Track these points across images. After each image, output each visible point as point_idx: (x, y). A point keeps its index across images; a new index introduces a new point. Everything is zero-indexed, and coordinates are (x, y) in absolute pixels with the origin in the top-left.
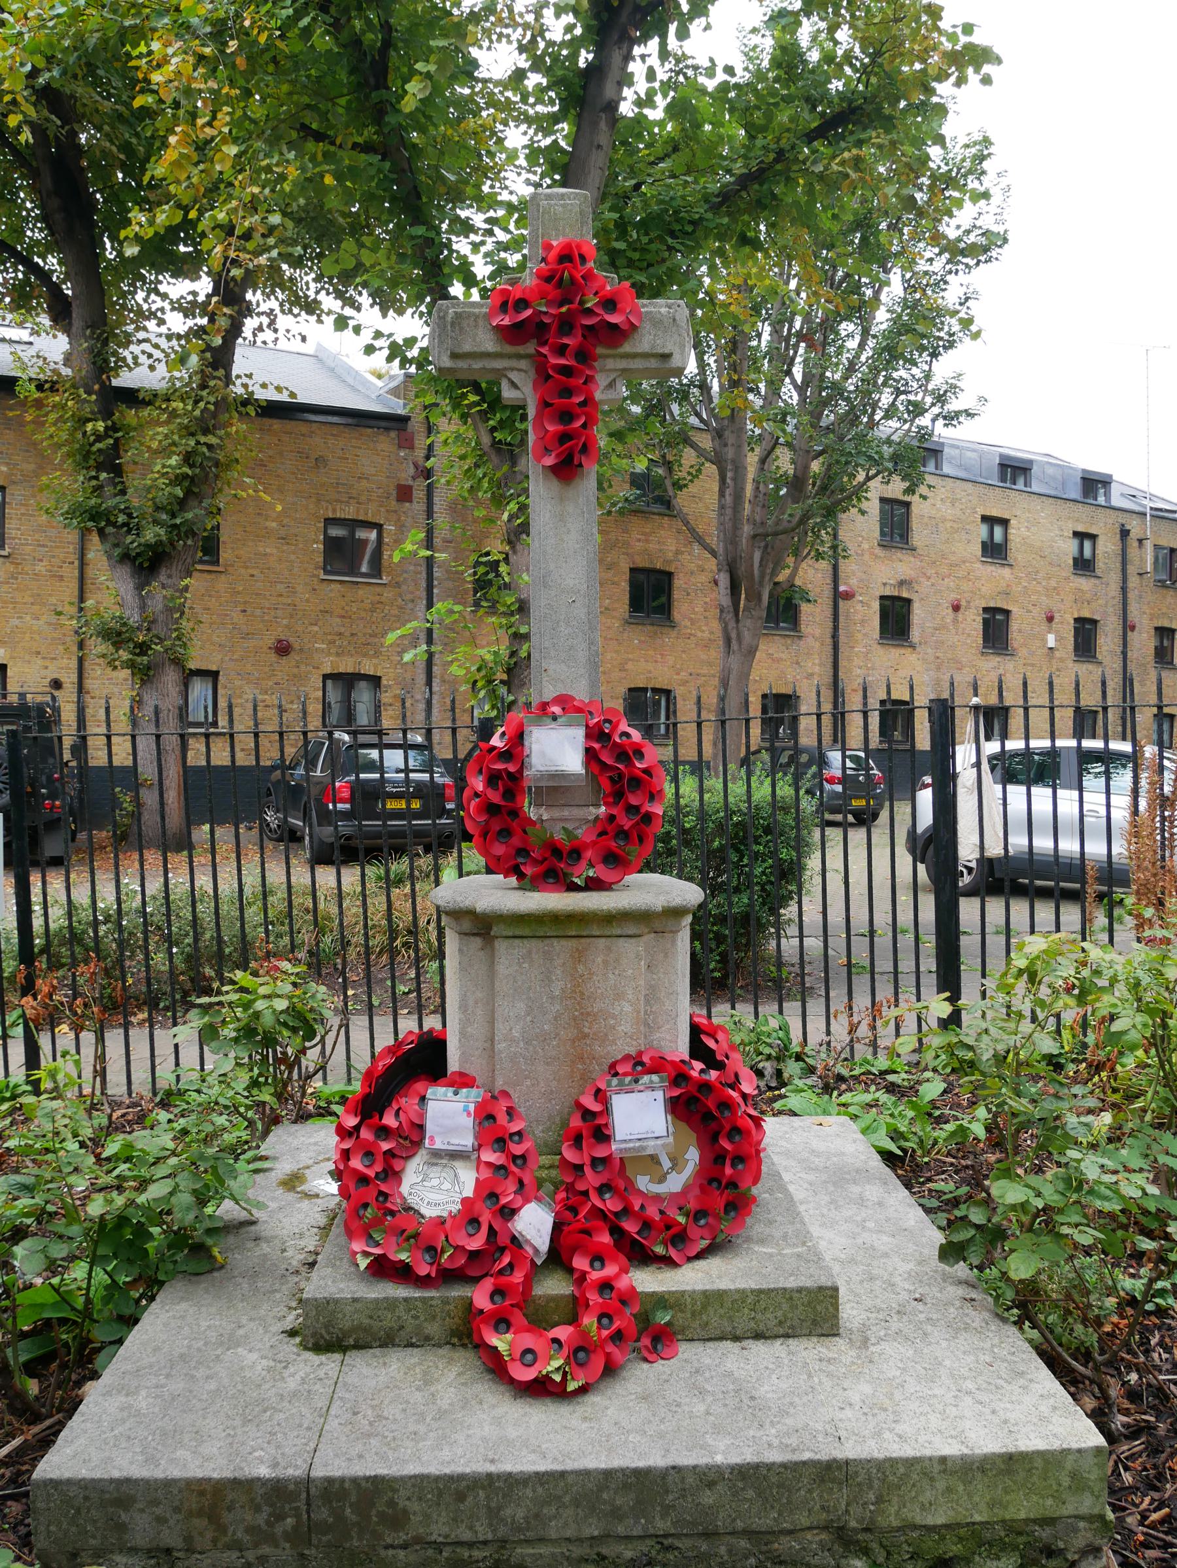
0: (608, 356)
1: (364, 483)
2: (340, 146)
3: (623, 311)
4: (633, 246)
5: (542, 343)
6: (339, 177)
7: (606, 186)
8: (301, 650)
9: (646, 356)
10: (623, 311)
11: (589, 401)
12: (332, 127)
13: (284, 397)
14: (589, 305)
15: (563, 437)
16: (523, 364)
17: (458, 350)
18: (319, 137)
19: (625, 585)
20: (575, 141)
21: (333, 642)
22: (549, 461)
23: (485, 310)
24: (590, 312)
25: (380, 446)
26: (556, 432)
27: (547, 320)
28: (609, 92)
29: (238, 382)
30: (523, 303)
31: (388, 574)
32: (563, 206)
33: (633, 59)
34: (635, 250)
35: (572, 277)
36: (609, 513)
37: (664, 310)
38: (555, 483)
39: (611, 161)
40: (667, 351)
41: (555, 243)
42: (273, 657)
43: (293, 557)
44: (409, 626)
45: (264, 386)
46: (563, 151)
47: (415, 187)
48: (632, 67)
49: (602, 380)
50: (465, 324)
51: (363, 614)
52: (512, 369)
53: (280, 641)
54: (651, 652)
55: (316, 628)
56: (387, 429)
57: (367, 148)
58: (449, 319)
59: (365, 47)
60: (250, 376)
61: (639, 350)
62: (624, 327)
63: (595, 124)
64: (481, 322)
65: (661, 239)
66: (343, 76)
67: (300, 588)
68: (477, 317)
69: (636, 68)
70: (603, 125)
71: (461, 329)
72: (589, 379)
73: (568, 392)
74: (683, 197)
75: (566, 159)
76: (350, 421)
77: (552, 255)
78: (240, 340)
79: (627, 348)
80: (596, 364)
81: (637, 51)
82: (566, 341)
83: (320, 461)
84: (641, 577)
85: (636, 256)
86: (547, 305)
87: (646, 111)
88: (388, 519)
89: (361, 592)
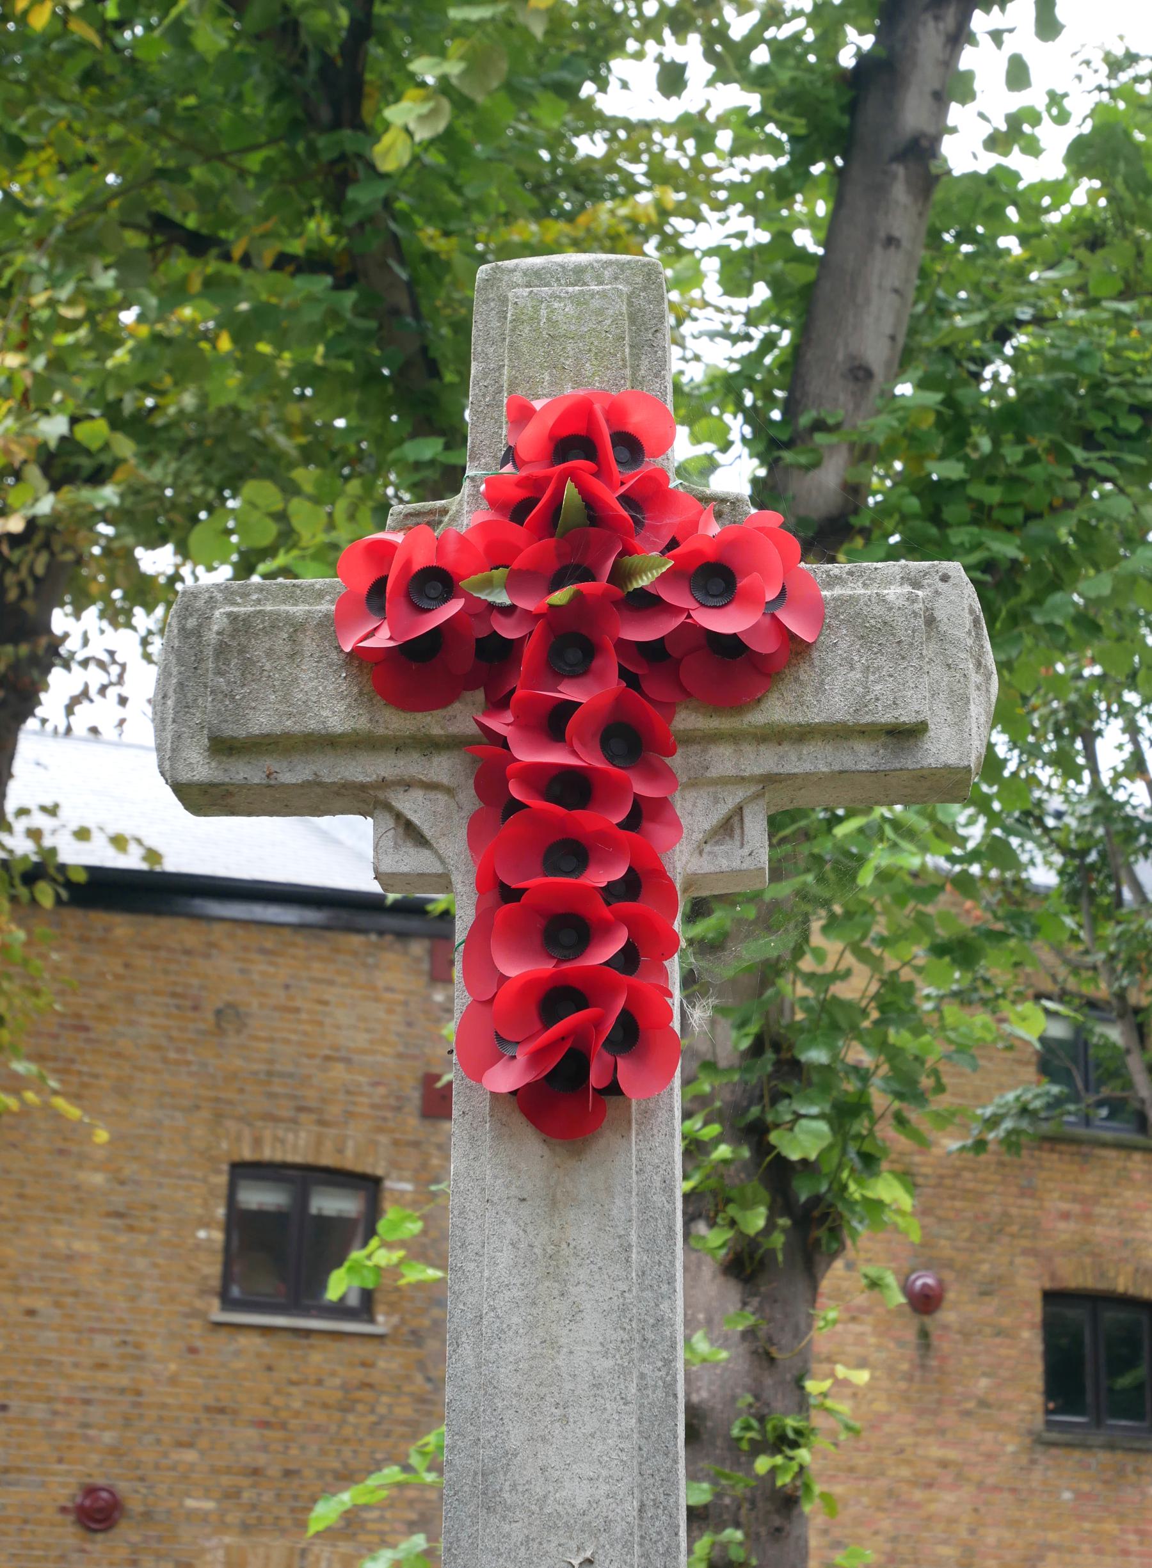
0: (714, 738)
1: (339, 1071)
2: (246, 261)
3: (752, 598)
4: (983, 470)
5: (497, 704)
6: (242, 331)
7: (912, 332)
8: (147, 1516)
9: (838, 733)
10: (752, 598)
11: (644, 880)
12: (228, 224)
13: (132, 860)
14: (644, 581)
15: (556, 998)
16: (442, 768)
17: (230, 730)
18: (198, 244)
19: (1031, 1339)
20: (831, 234)
21: (232, 1494)
22: (507, 1077)
23: (327, 607)
24: (647, 603)
25: (383, 979)
26: (529, 985)
27: (509, 631)
28: (913, 115)
29: (20, 825)
30: (437, 581)
31: (393, 1308)
32: (576, 300)
33: (971, 39)
34: (991, 481)
35: (590, 500)
36: (980, 1145)
37: (895, 593)
38: (532, 1149)
39: (923, 274)
40: (906, 717)
41: (538, 405)
42: (69, 1534)
43: (141, 1263)
44: (373, 1481)
45: (82, 834)
46: (801, 255)
47: (424, 350)
48: (968, 59)
49: (694, 812)
50: (258, 649)
51: (319, 1417)
52: (407, 784)
53: (91, 1491)
54: (1111, 1527)
55: (190, 1456)
56: (403, 936)
57: (313, 263)
58: (211, 636)
59: (305, 39)
60: (51, 811)
61: (816, 717)
62: (765, 646)
63: (879, 192)
64: (309, 644)
65: (1059, 453)
66: (256, 106)
67: (154, 1348)
68: (297, 627)
69: (980, 61)
70: (900, 192)
71: (247, 665)
72: (646, 814)
73: (576, 852)
74: (1115, 352)
75: (809, 274)
76: (311, 915)
77: (532, 436)
78: (31, 724)
79: (775, 710)
80: (675, 762)
81: (980, 22)
82: (569, 692)
83: (229, 1017)
84: (1076, 1314)
85: (993, 495)
86: (510, 586)
87: (1016, 160)
88: (394, 1164)
89: (316, 1357)
